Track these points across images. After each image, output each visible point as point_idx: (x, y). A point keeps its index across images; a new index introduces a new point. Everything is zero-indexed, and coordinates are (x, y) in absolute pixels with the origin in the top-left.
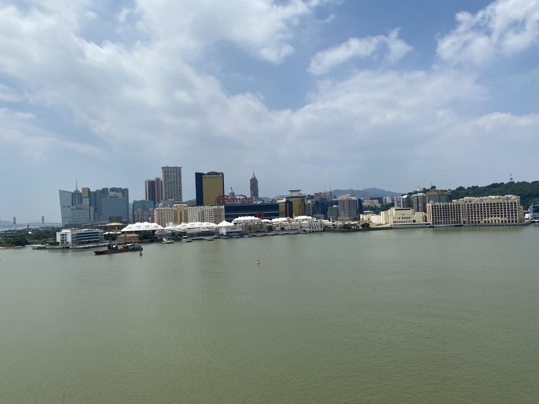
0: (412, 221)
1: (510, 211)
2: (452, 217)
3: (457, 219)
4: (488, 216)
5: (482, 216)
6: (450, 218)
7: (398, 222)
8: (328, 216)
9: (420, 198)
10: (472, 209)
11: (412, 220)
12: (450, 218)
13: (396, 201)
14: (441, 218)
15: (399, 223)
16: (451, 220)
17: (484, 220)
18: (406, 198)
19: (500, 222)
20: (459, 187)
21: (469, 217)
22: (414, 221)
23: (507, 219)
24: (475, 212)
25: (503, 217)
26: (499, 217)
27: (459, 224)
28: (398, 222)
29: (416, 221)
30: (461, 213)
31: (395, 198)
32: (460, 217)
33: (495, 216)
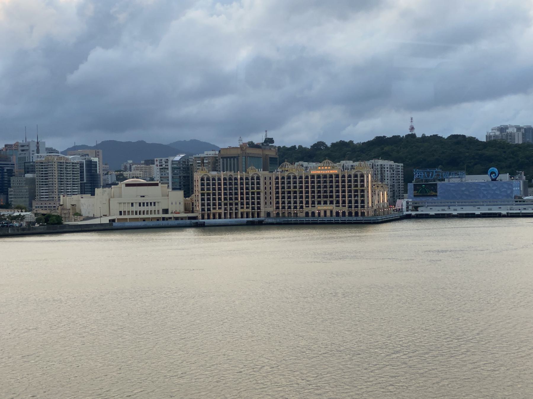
0: (161, 211)
1: (250, 194)
2: (242, 204)
3: (253, 208)
4: (313, 203)
5: (301, 202)
6: (239, 204)
7: (129, 212)
8: (11, 195)
9: (207, 161)
10: (283, 188)
11: (160, 207)
12: (239, 204)
13: (159, 167)
14: (220, 204)
15: (132, 214)
16: (240, 211)
17: (305, 209)
18: (179, 162)
19: (334, 214)
20: (335, 142)
21: (278, 203)
22: (166, 211)
23: (346, 209)
24: (289, 192)
25: (341, 205)
26: (333, 204)
27: (256, 219)
28: (125, 212)
29: (170, 211)
30: (262, 195)
31: (157, 160)
32: (259, 203)
33: (325, 203)
